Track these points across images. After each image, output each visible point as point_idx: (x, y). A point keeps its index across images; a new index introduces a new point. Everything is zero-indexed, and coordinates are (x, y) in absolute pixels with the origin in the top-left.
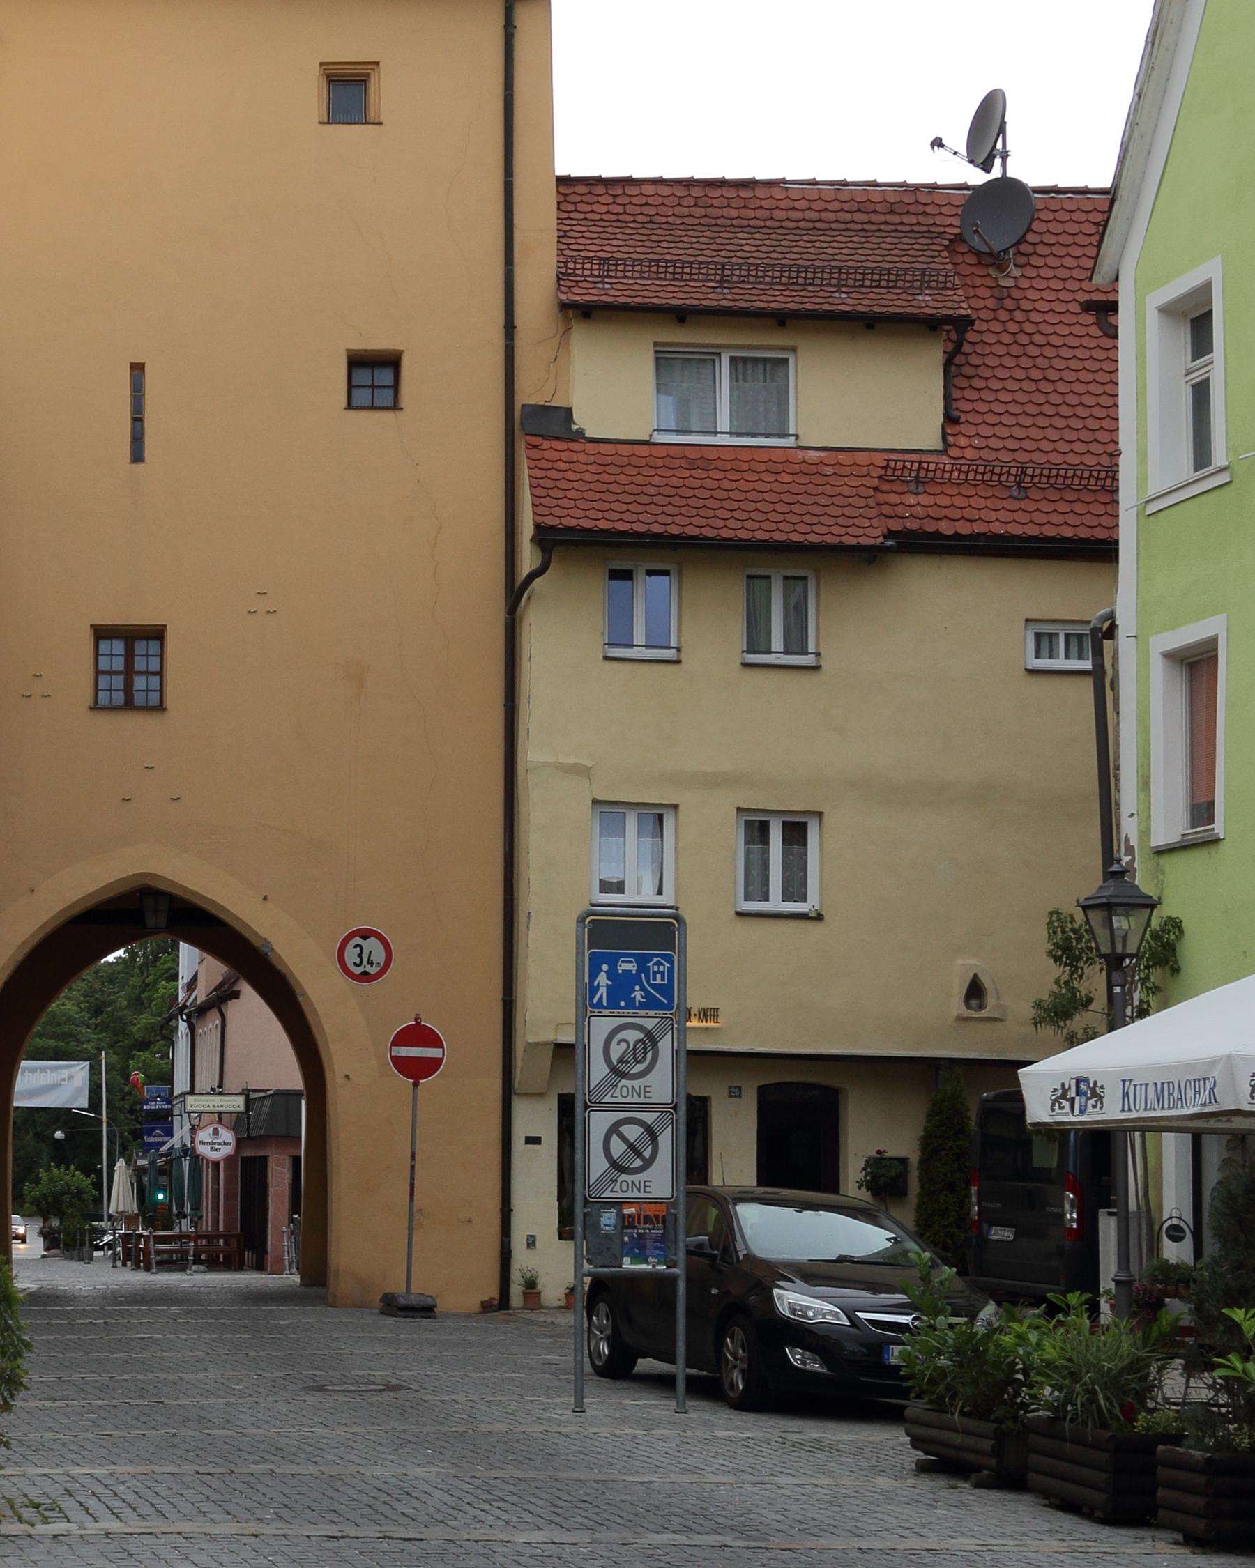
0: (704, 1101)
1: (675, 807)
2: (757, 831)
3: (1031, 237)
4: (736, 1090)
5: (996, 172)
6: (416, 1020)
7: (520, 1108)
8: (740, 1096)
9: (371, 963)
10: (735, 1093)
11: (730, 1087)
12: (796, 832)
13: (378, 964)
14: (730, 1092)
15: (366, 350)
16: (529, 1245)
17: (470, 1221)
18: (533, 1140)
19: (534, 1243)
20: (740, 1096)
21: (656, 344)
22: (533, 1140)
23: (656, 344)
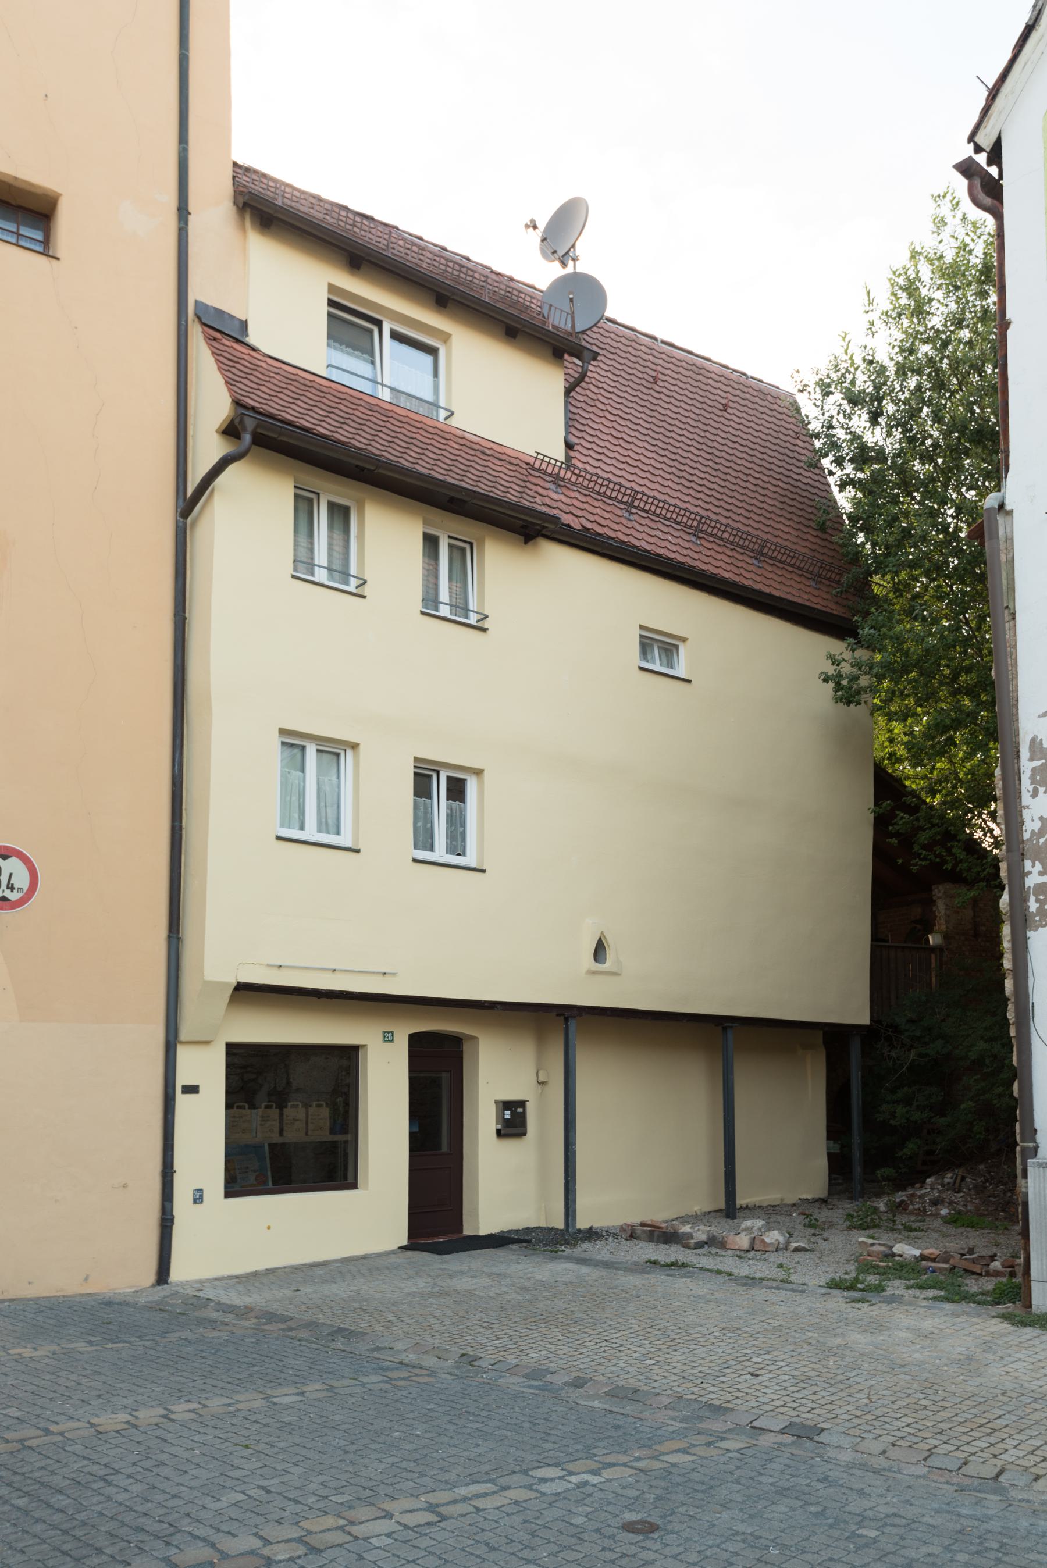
0: (184, 1087)
1: (355, 746)
2: (422, 784)
3: (595, 329)
4: (390, 1035)
5: (570, 269)
6: (825, 680)
7: (184, 1055)
8: (392, 1041)
9: (12, 888)
10: (388, 1038)
11: (384, 1033)
12: (457, 790)
13: (20, 889)
14: (385, 1037)
15: (16, 178)
16: (195, 1202)
17: (125, 1186)
18: (191, 1089)
19: (201, 1197)
20: (392, 1041)
21: (332, 288)
22: (191, 1089)
23: (332, 288)
